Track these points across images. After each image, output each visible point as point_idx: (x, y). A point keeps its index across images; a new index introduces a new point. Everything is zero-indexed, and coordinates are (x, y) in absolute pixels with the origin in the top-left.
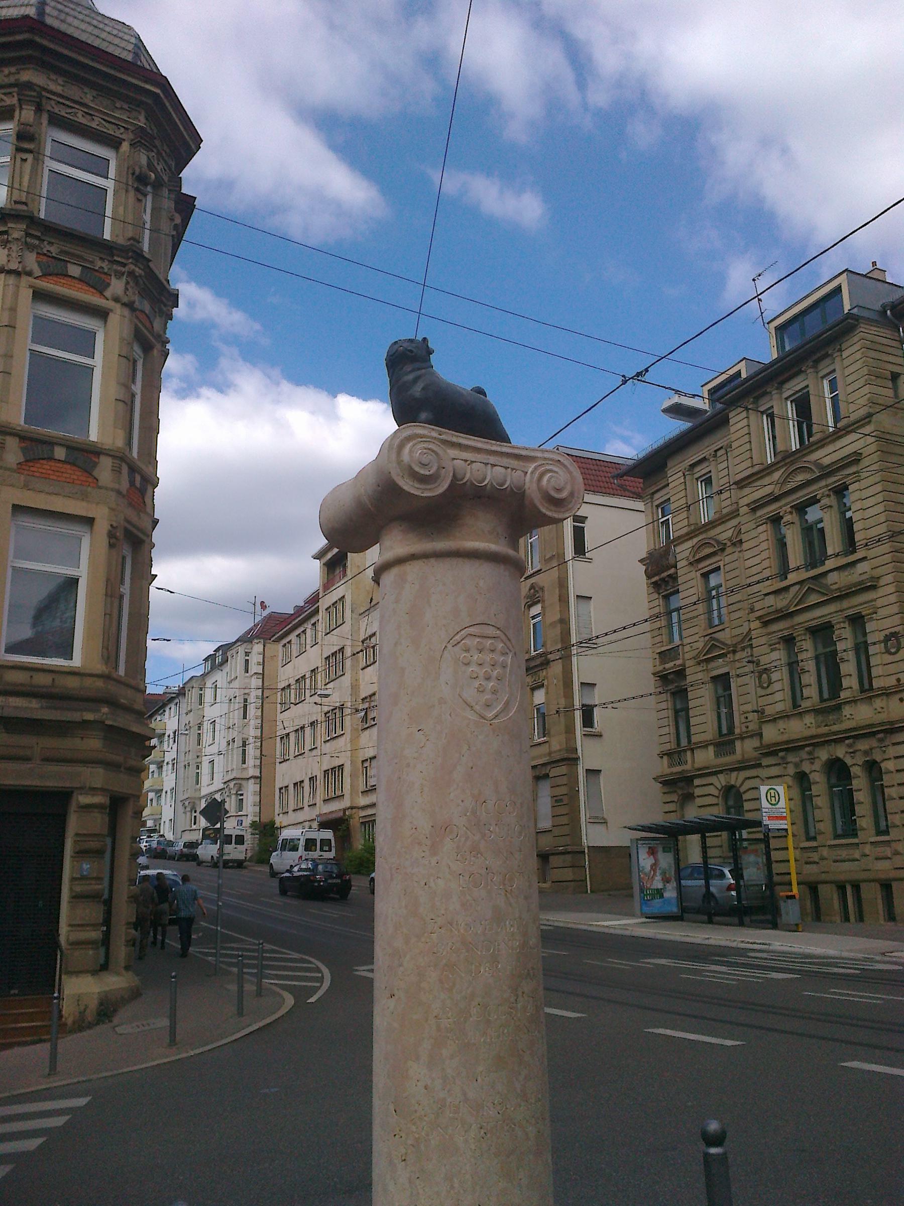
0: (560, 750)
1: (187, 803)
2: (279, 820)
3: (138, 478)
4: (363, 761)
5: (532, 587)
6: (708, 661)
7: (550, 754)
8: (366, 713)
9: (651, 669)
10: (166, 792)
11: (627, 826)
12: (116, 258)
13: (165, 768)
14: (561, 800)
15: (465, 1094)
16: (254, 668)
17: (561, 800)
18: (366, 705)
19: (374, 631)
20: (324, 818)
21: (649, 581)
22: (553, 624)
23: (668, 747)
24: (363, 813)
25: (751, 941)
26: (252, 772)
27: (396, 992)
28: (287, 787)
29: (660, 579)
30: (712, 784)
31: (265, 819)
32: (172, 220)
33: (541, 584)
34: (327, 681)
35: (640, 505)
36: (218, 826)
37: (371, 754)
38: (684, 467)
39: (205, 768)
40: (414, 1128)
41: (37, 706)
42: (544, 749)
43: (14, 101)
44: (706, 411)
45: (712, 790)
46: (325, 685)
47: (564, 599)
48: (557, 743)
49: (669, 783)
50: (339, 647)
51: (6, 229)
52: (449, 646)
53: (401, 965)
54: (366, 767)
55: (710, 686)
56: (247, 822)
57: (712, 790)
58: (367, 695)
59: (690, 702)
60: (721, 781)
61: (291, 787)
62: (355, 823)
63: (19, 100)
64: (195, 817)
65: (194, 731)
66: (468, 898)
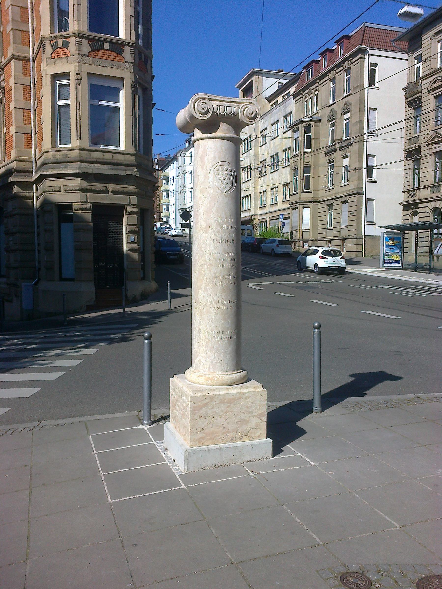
0: (354, 189)
1: (180, 211)
3: (143, 56)
4: (260, 193)
5: (346, 103)
6: (432, 144)
7: (349, 190)
8: (262, 168)
9: (403, 148)
10: (171, 206)
11: (380, 226)
13: (170, 194)
14: (353, 213)
15: (213, 298)
17: (353, 213)
18: (262, 165)
19: (266, 127)
21: (407, 101)
22: (355, 124)
23: (408, 188)
25: (430, 280)
27: (196, 272)
29: (412, 100)
30: (427, 207)
33: (351, 102)
34: (243, 153)
35: (405, 56)
36: (188, 222)
37: (264, 190)
38: (431, 35)
40: (200, 307)
41: (107, 168)
42: (347, 188)
44: (421, 15)
45: (427, 210)
47: (361, 110)
48: (353, 186)
49: (406, 207)
50: (249, 135)
53: (197, 264)
54: (262, 196)
55: (433, 157)
57: (427, 210)
58: (262, 160)
59: (421, 165)
60: (432, 205)
62: (256, 221)
65: (182, 177)
66: (216, 246)
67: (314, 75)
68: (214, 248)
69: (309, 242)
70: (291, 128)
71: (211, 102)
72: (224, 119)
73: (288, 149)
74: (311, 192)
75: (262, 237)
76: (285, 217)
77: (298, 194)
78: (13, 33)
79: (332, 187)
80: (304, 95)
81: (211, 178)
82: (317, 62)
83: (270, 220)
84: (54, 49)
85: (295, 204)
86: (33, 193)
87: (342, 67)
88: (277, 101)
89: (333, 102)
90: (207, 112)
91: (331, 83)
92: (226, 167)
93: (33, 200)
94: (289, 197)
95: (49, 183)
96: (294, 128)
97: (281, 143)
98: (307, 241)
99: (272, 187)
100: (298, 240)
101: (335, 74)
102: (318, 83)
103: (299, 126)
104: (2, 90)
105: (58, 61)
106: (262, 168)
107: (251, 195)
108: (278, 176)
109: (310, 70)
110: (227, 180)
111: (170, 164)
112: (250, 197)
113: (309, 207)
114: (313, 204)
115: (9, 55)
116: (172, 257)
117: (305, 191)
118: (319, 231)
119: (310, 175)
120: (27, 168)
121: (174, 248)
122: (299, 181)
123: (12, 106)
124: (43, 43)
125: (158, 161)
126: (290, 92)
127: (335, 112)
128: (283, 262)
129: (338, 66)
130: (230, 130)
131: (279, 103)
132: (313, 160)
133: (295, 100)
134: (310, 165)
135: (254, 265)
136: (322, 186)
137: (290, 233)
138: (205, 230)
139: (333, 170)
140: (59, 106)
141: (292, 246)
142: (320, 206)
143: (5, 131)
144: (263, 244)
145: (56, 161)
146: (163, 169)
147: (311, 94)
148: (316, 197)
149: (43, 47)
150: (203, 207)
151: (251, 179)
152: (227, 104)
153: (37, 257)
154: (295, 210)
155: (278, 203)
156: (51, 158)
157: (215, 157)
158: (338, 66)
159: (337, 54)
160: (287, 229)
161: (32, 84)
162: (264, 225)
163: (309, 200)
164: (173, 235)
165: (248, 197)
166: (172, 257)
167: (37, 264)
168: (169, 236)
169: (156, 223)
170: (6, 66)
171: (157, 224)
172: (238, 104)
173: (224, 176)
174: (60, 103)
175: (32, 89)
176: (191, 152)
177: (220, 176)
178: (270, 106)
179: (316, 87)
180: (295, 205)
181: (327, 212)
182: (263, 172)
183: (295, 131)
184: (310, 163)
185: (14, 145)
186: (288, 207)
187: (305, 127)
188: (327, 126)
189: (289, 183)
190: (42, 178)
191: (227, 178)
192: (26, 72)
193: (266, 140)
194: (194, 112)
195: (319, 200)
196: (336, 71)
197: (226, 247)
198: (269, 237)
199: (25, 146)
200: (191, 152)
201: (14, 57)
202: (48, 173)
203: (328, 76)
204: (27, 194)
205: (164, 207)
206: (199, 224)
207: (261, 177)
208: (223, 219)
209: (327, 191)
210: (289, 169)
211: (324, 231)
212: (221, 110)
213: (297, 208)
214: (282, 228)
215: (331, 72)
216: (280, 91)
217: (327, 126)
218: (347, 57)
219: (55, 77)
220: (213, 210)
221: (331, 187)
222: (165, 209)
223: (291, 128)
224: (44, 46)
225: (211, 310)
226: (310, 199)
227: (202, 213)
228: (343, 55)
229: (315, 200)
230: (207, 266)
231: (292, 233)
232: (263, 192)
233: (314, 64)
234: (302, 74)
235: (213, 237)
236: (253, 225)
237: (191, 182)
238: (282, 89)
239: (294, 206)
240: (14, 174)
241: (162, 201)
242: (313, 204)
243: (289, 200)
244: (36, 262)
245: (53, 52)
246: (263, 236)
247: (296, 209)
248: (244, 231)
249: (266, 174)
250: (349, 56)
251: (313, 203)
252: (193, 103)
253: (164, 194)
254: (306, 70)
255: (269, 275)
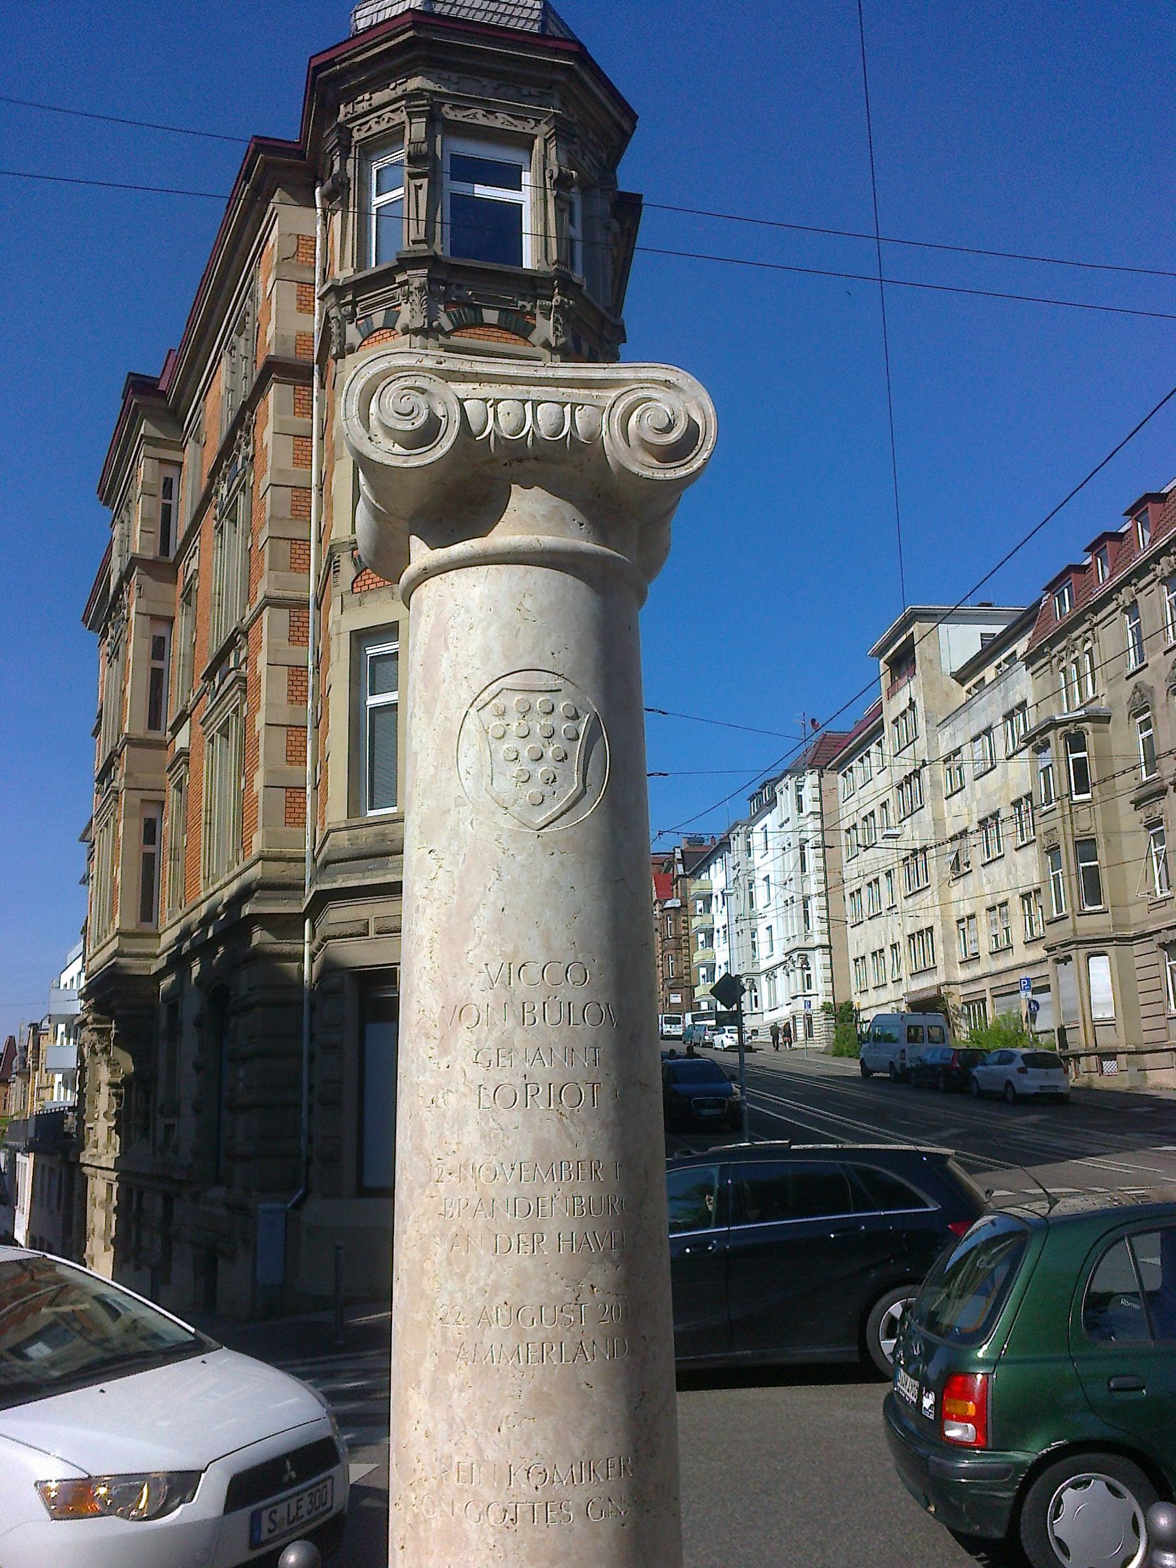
2: (859, 1001)
4: (959, 922)
10: (720, 967)
12: (539, 291)
15: (480, 1451)
16: (809, 806)
20: (914, 998)
24: (962, 991)
26: (817, 939)
28: (863, 958)
31: (840, 1000)
32: (608, 229)
36: (735, 1008)
37: (969, 912)
39: (762, 936)
43: (404, 116)
46: (900, 822)
51: (406, 278)
52: (473, 711)
54: (963, 929)
56: (816, 1003)
61: (869, 957)
63: (408, 113)
64: (756, 997)
66: (492, 1124)
67: (1075, 602)
68: (483, 1137)
69: (1118, 1055)
70: (1028, 741)
71: (453, 386)
72: (526, 464)
73: (1024, 799)
74: (1108, 912)
75: (976, 1047)
76: (1037, 986)
77: (1067, 917)
78: (270, 543)
79: (1167, 894)
80: (1055, 656)
81: (470, 755)
82: (1081, 569)
83: (995, 996)
84: (361, 570)
85: (1062, 946)
86: (304, 944)
87: (1152, 574)
88: (983, 678)
89: (1139, 666)
90: (428, 433)
91: (1127, 617)
92: (541, 698)
93: (303, 963)
94: (1042, 930)
95: (338, 915)
96: (1036, 741)
97: (1005, 785)
98: (1111, 1055)
99: (990, 904)
100: (1084, 1052)
101: (1134, 593)
102: (1088, 622)
103: (1051, 735)
104: (241, 683)
105: (370, 597)
106: (957, 854)
107: (932, 927)
108: (1004, 870)
109: (1063, 591)
110: (554, 763)
111: (713, 859)
112: (929, 934)
113: (1106, 955)
114: (1115, 945)
115: (260, 597)
116: (706, 1112)
117: (1088, 909)
118: (1146, 1024)
119: (1096, 863)
120: (291, 877)
121: (713, 1086)
122: (1066, 879)
123: (260, 720)
124: (335, 557)
125: (685, 855)
126: (1014, 653)
127: (1147, 690)
128: (1040, 1120)
129: (1142, 570)
130: (563, 518)
131: (987, 682)
132: (1100, 821)
133: (1030, 671)
134: (1093, 837)
135: (954, 1131)
136: (1136, 891)
137: (1056, 1031)
138: (438, 1034)
139: (1164, 847)
140: (370, 709)
141: (1066, 1071)
142: (1137, 949)
143: (243, 787)
144: (979, 1068)
145: (358, 852)
146: (695, 874)
147: (1074, 652)
148: (1120, 925)
149: (334, 568)
150: (430, 911)
151: (929, 886)
152: (535, 392)
153: (305, 1124)
154: (1066, 964)
155: (1012, 947)
156: (346, 846)
157: (487, 652)
158: (1142, 570)
159: (1135, 542)
160: (1046, 1021)
161: (310, 663)
162: (979, 1012)
163: (1104, 933)
164: (726, 1046)
165: (924, 936)
166: (706, 1112)
167: (303, 1141)
168: (716, 1049)
169: (681, 1016)
170: (252, 625)
171: (684, 1018)
172: (595, 393)
173: (536, 742)
174: (373, 701)
175: (311, 676)
176: (766, 826)
177: (511, 743)
178: (965, 694)
179: (1085, 632)
180: (1063, 949)
181: (1162, 966)
182: (962, 866)
183: (1038, 750)
184: (1092, 831)
185: (260, 819)
186: (1044, 956)
187: (1067, 736)
188: (1129, 727)
189: (1038, 891)
190: (322, 900)
191: (549, 753)
192: (297, 634)
193: (961, 780)
194: (361, 438)
195: (1131, 933)
196: (1135, 585)
197: (551, 1131)
198: (994, 1045)
199: (288, 820)
200: (766, 826)
201: (270, 602)
202: (335, 886)
203: (1117, 599)
204: (286, 948)
205: (703, 971)
206: (414, 1000)
207: (956, 878)
208: (534, 970)
209: (1153, 907)
210: (1032, 852)
211: (1161, 1022)
212: (505, 420)
213: (1071, 959)
214: (1032, 1017)
215: (1123, 590)
216: (987, 654)
217: (1129, 727)
218: (1163, 546)
219: (360, 638)
220: (476, 922)
221: (1163, 895)
222: (703, 977)
223: (1028, 741)
224: (337, 564)
225: (470, 1526)
226: (1106, 930)
227: (426, 943)
228: (1152, 541)
229: (1119, 934)
230: (446, 1246)
231: (1062, 1032)
232: (966, 919)
233: (1072, 575)
234: (1043, 605)
235: (476, 1074)
236: (946, 1012)
237: (767, 903)
238: (991, 648)
239: (1060, 954)
240: (256, 895)
241: (697, 957)
242: (1115, 945)
243: (1044, 937)
244: (302, 1138)
245: (357, 577)
246: (979, 1043)
247: (1068, 963)
248: (920, 1030)
249: (969, 869)
250: (1168, 543)
251: (1115, 942)
252: (355, 399)
253: (701, 937)
254: (1053, 593)
255: (996, 1165)
